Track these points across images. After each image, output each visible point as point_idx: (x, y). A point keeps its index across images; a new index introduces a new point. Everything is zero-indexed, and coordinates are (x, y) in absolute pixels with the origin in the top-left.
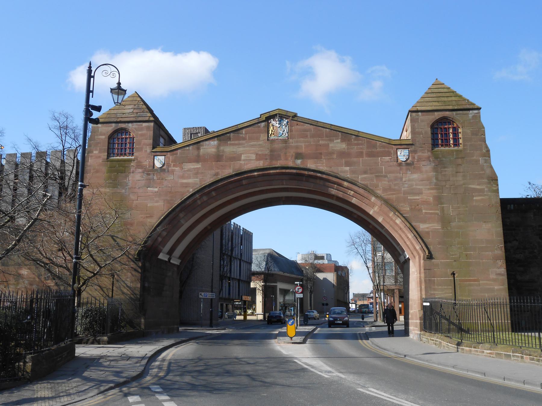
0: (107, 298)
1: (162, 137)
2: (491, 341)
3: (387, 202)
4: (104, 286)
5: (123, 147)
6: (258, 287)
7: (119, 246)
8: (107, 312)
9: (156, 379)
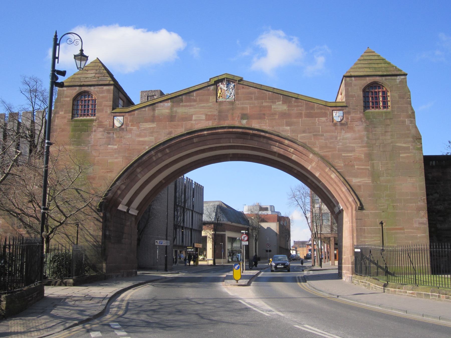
0: (73, 244)
1: (121, 99)
2: (413, 282)
3: (323, 159)
4: (70, 234)
5: (86, 108)
6: (208, 235)
7: (83, 198)
8: (72, 257)
9: (116, 317)
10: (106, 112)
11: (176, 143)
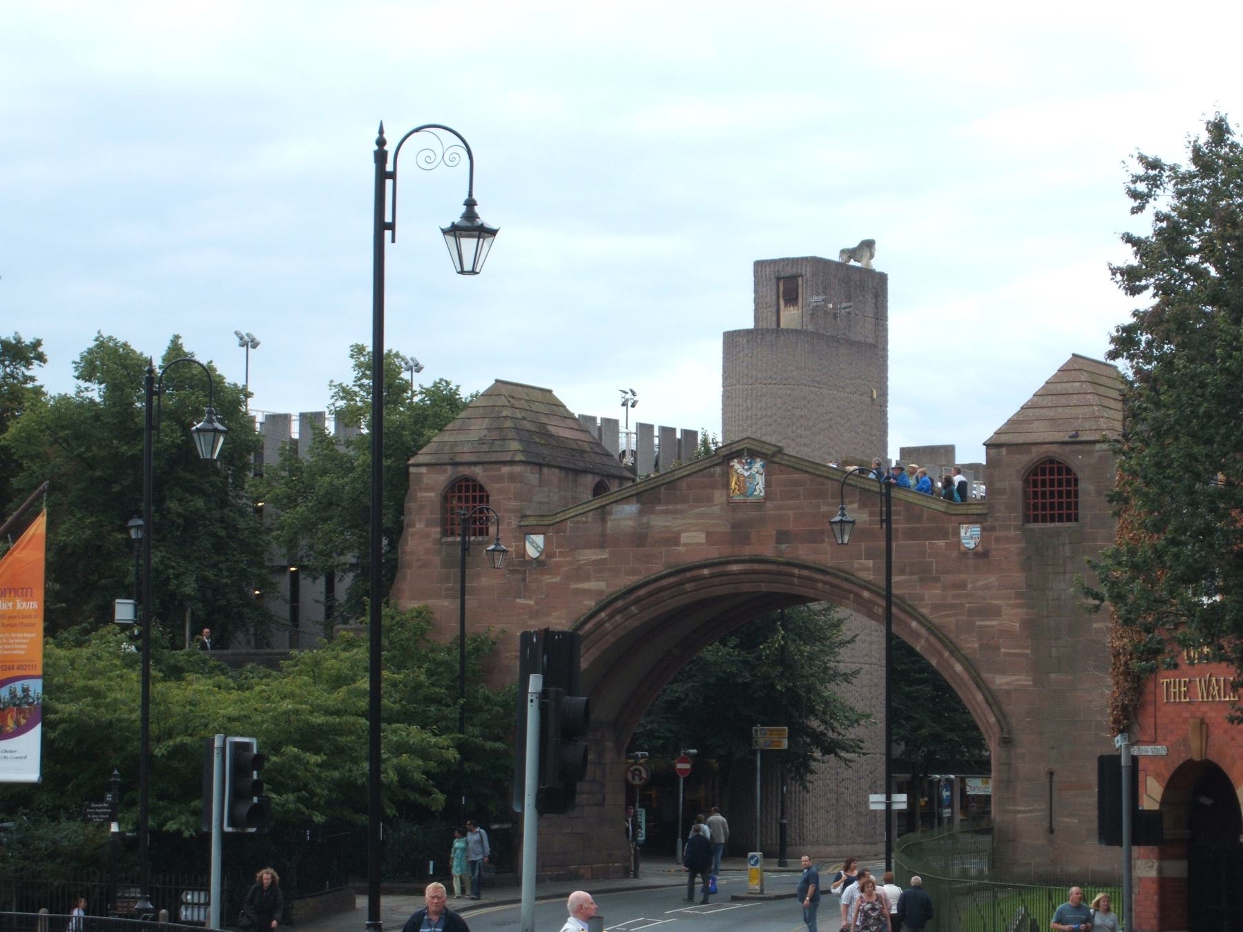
10: (509, 524)
11: (650, 594)
